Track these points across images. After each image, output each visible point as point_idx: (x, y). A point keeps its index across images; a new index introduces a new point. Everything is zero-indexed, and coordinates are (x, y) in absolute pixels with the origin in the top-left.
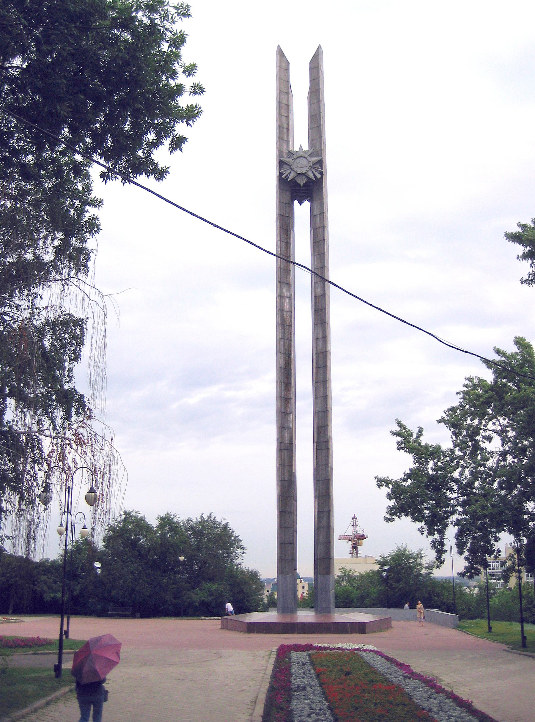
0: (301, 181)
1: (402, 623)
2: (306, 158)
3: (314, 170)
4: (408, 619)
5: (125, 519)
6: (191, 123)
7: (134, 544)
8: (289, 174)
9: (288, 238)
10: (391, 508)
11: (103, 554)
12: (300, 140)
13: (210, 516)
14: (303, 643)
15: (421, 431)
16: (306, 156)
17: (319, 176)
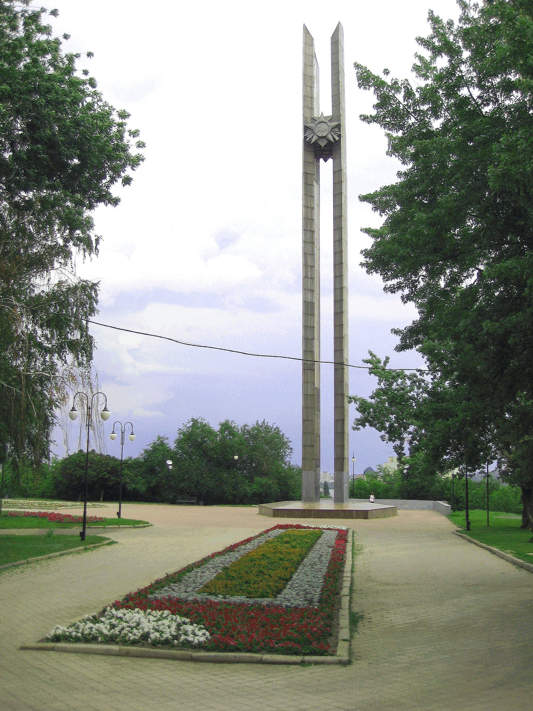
0: (323, 143)
1: (404, 511)
2: (326, 123)
3: (333, 133)
4: (423, 509)
5: (193, 425)
6: (135, 168)
7: (199, 446)
8: (312, 137)
9: (312, 191)
10: (358, 420)
11: (176, 453)
12: (325, 108)
13: (264, 422)
14: (294, 524)
15: (387, 359)
16: (326, 121)
17: (337, 138)
